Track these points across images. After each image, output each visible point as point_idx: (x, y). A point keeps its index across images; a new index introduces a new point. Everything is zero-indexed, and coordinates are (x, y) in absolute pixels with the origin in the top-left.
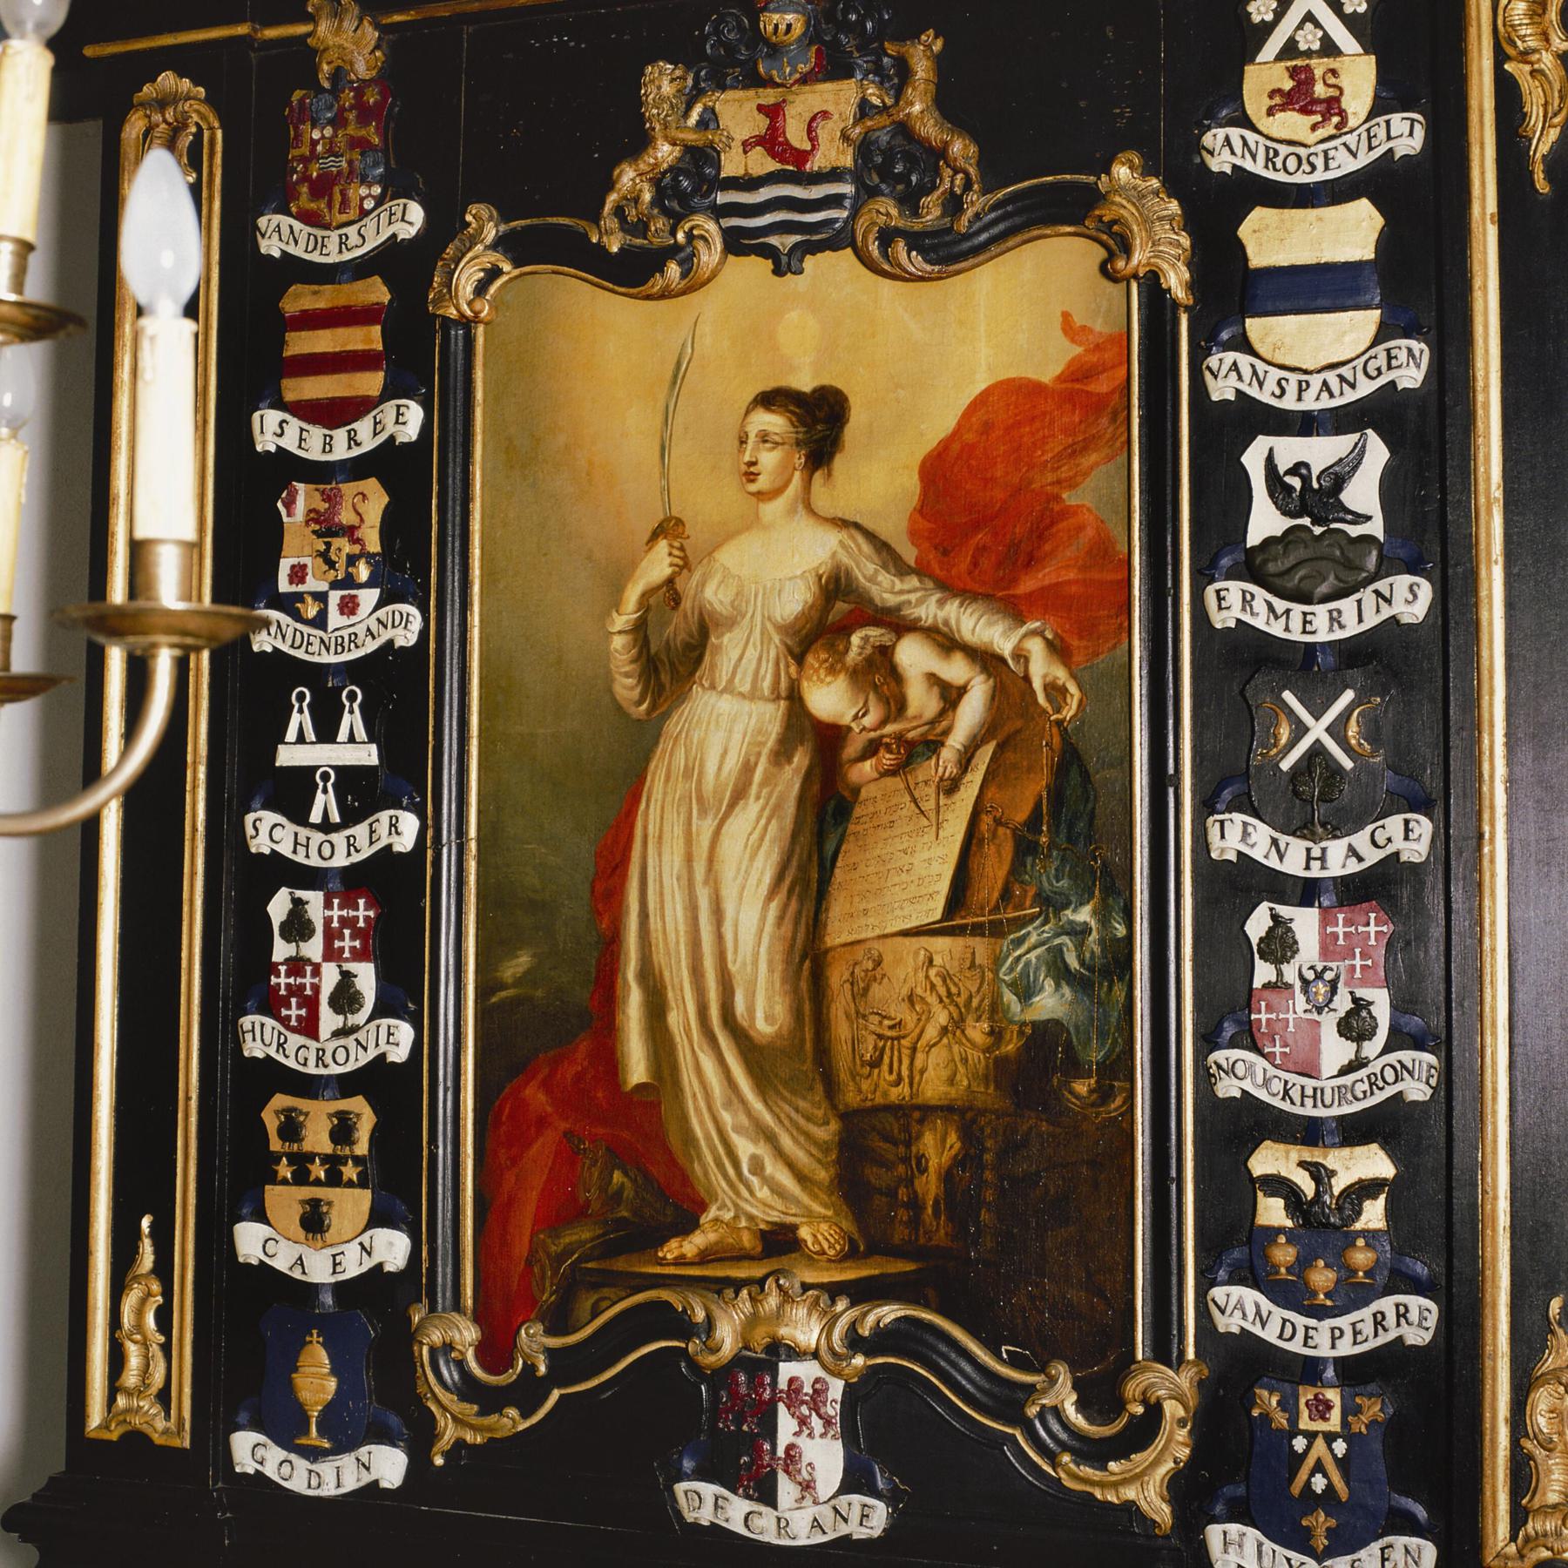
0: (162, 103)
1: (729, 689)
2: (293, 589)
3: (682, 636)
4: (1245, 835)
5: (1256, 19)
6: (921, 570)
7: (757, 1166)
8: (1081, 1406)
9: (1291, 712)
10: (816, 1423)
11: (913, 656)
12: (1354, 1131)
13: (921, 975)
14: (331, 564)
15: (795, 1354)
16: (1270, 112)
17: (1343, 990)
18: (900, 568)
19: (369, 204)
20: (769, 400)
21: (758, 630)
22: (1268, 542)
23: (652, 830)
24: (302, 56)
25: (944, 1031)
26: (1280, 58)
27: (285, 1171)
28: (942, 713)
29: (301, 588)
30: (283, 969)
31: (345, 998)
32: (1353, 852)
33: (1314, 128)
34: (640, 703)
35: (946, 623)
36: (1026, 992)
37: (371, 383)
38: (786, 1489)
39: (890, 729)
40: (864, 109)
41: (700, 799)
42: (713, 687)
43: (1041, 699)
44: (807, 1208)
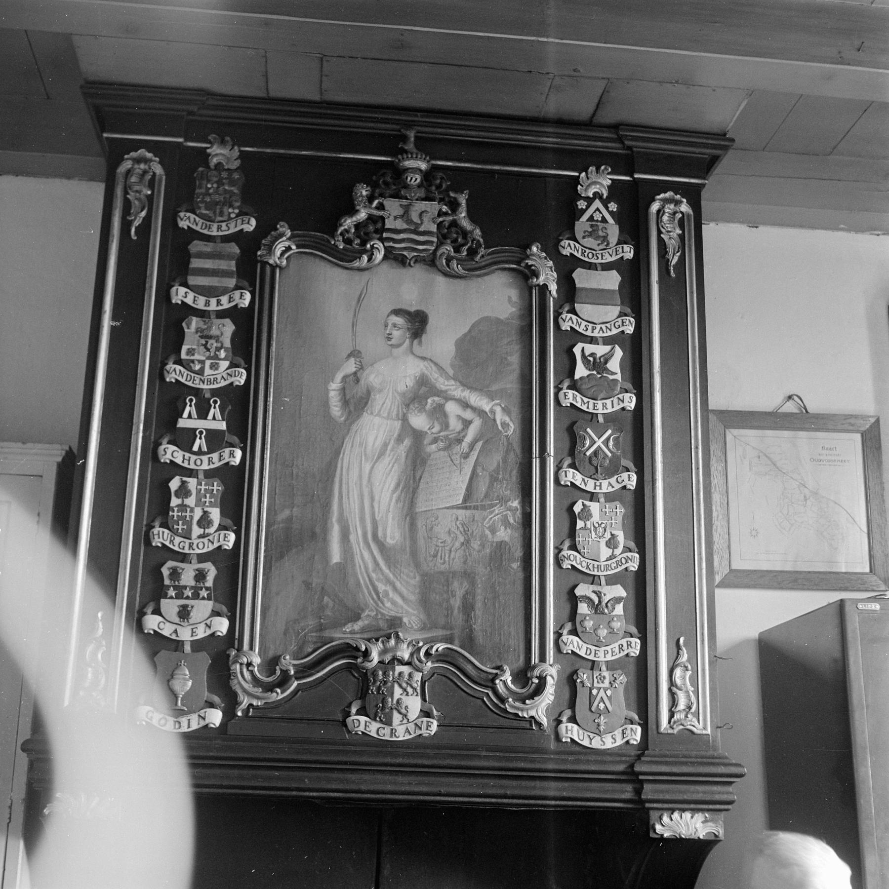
0: (138, 161)
1: (378, 415)
2: (188, 357)
3: (360, 394)
4: (574, 477)
5: (580, 207)
6: (455, 378)
7: (386, 594)
8: (513, 682)
9: (590, 436)
10: (409, 690)
11: (451, 408)
12: (612, 580)
13: (454, 524)
14: (208, 350)
15: (402, 662)
16: (584, 237)
17: (608, 531)
18: (448, 378)
19: (233, 216)
20: (397, 312)
21: (391, 394)
22: (581, 378)
23: (345, 465)
24: (203, 156)
25: (463, 544)
26: (588, 220)
27: (172, 592)
28: (463, 430)
29: (192, 358)
30: (176, 509)
31: (205, 521)
32: (610, 484)
33: (599, 245)
34: (340, 417)
35: (465, 398)
36: (493, 531)
37: (232, 282)
38: (396, 717)
39: (442, 434)
40: (441, 214)
41: (366, 455)
42: (372, 413)
43: (500, 428)
44: (406, 611)
